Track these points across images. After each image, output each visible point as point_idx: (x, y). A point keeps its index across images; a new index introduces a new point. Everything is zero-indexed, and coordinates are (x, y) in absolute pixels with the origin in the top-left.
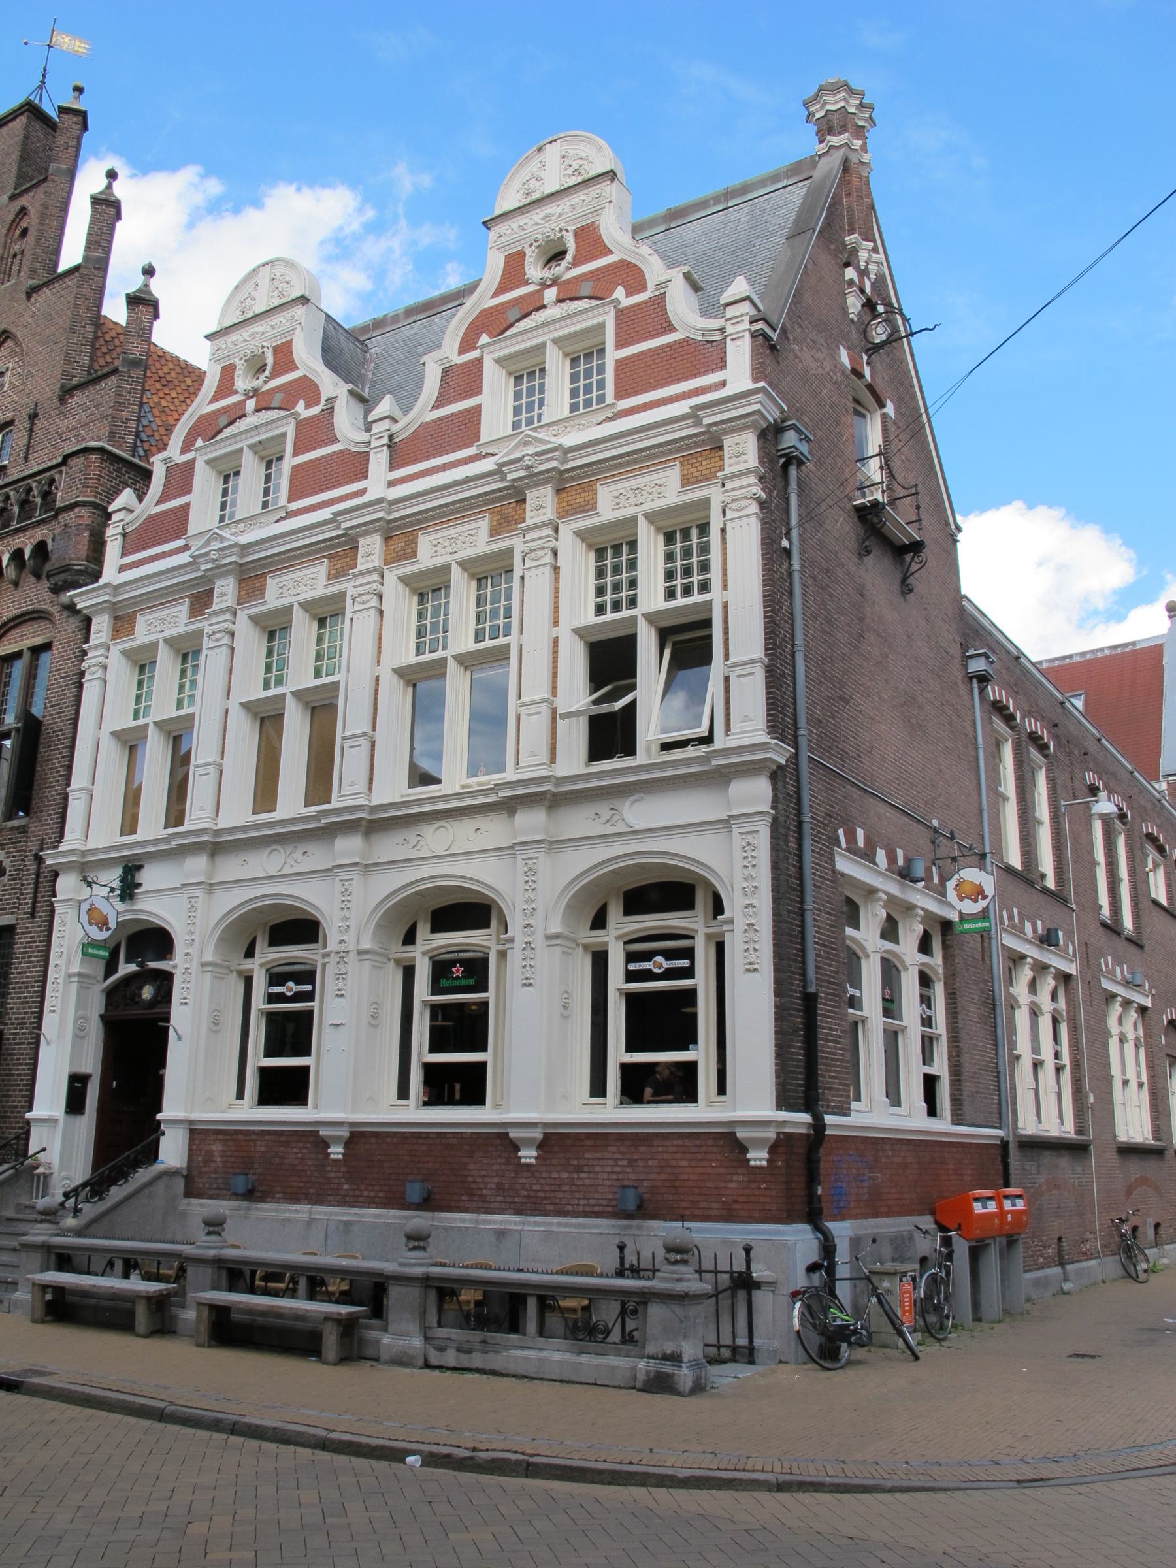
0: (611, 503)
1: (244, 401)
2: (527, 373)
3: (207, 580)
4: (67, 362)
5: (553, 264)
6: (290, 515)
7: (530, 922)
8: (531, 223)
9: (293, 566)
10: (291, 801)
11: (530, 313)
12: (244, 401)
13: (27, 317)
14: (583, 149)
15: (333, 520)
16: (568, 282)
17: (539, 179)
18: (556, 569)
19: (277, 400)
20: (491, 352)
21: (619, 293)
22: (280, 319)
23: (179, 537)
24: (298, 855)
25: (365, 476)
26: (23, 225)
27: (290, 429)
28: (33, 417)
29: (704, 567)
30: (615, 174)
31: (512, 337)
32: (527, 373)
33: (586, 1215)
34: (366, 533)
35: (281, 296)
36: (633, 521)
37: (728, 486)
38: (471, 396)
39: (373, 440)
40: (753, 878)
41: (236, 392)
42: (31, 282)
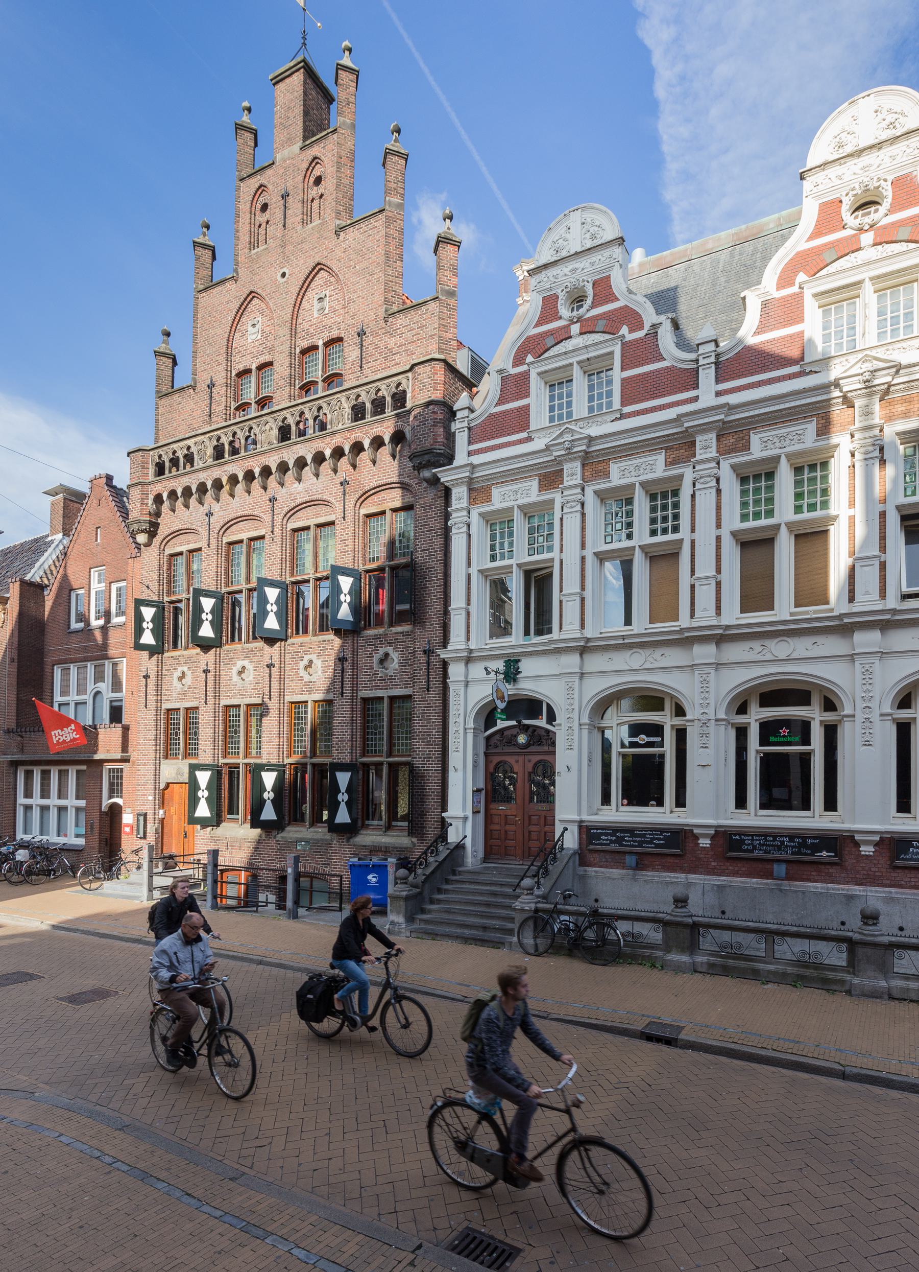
0: (619, 474)
1: (569, 325)
2: (558, 382)
3: (558, 461)
4: (386, 291)
5: (860, 213)
6: (623, 416)
7: (869, 705)
8: (562, 274)
9: (632, 455)
10: (784, 607)
11: (561, 341)
12: (569, 325)
13: (339, 252)
14: (600, 219)
15: (679, 419)
16: (885, 227)
17: (566, 240)
18: (719, 491)
19: (601, 325)
20: (810, 288)
21: (624, 330)
22: (599, 258)
23: (522, 431)
25: (696, 387)
26: (262, 200)
27: (617, 350)
28: (361, 334)
29: (676, 517)
30: (624, 241)
31: (546, 359)
32: (558, 382)
33: (911, 887)
34: (456, 485)
35: (593, 237)
36: (632, 486)
37: (697, 468)
38: (522, 398)
39: (701, 358)
40: (870, 691)
41: (560, 318)
42: (338, 222)
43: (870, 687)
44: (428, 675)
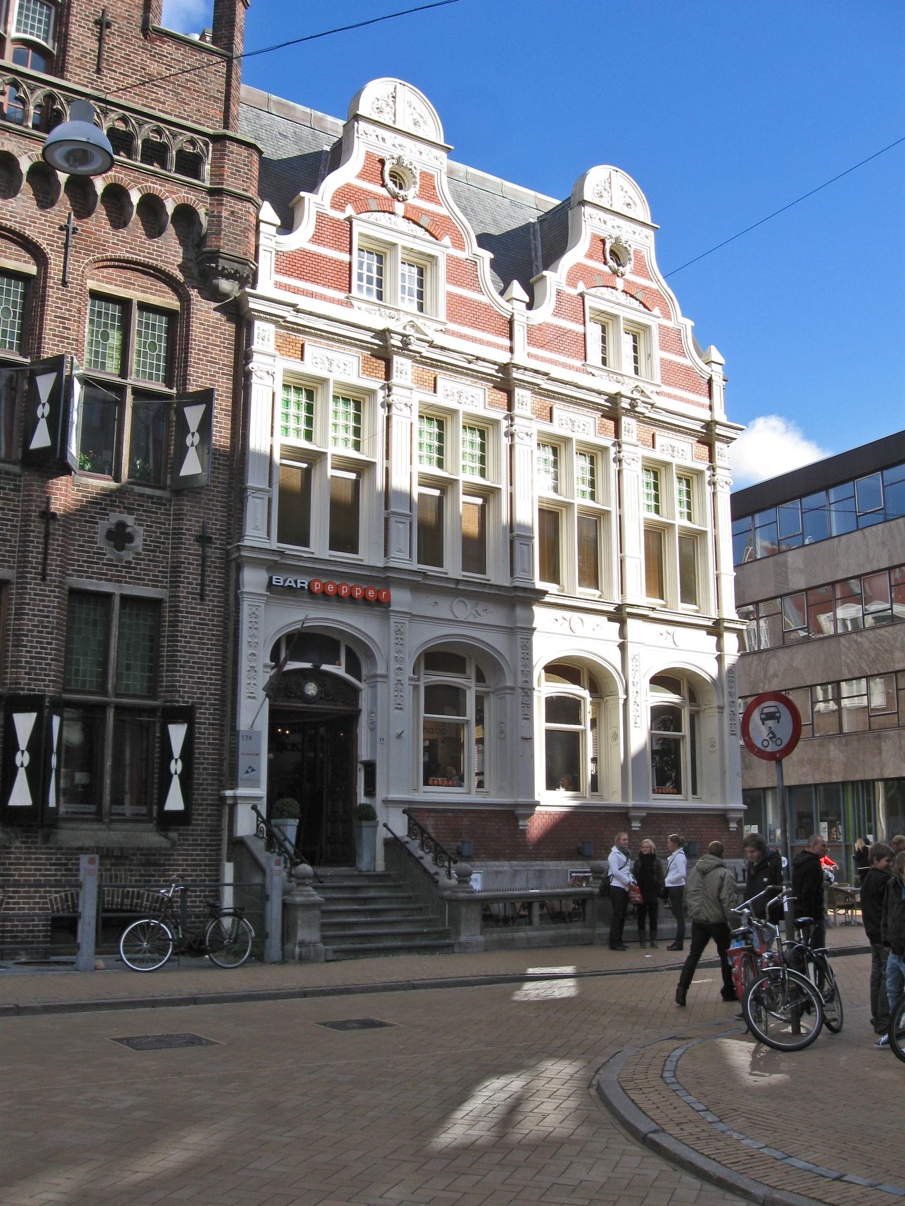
24: (480, 609)
43: (255, 632)
44: (202, 575)
